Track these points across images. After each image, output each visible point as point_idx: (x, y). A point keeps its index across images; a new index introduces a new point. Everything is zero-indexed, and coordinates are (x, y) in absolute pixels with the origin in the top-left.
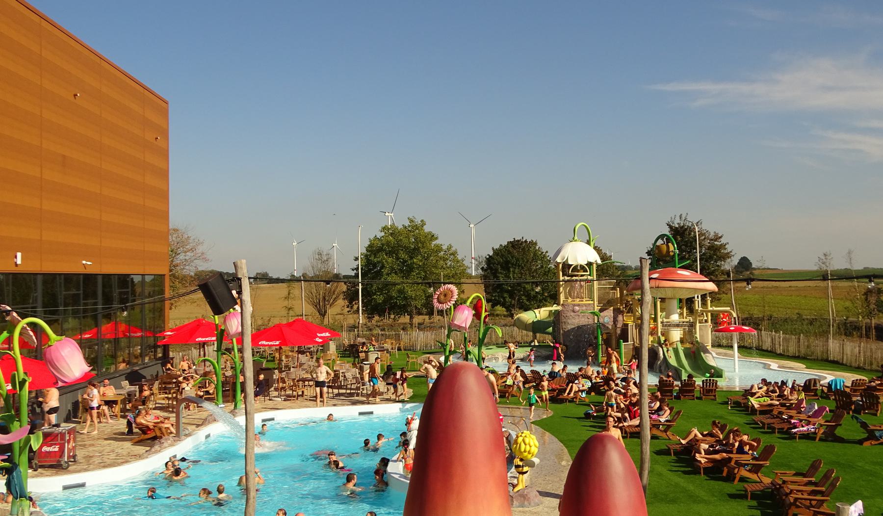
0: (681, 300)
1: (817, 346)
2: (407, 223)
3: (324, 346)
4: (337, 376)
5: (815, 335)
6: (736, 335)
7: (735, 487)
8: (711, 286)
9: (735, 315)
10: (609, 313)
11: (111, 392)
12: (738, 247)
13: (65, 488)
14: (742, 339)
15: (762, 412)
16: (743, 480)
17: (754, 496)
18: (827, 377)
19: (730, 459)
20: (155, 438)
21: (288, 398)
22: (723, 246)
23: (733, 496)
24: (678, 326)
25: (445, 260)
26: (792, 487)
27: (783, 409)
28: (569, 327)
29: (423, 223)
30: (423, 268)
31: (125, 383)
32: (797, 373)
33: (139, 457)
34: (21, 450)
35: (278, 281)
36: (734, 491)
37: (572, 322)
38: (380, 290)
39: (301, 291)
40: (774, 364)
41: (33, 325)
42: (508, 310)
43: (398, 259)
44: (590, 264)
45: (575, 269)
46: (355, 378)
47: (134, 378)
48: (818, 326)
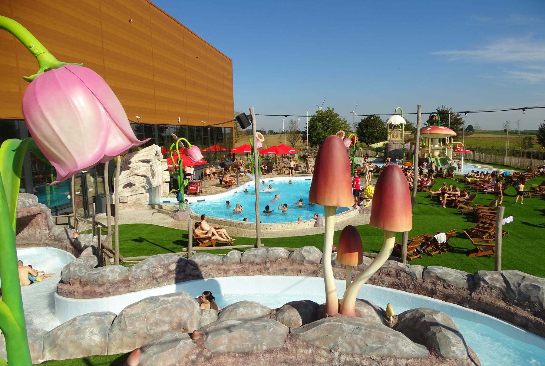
0: (440, 139)
1: (499, 160)
2: (327, 109)
3: (293, 155)
4: (297, 166)
5: (499, 155)
6: (463, 154)
7: (457, 210)
8: (453, 133)
9: (463, 145)
10: (409, 144)
11: (214, 170)
12: (467, 121)
13: (198, 201)
14: (466, 155)
15: (472, 184)
16: (461, 208)
17: (465, 214)
18: (502, 171)
19: (456, 199)
20: (230, 186)
21: (279, 174)
22: (461, 119)
23: (455, 214)
24: (438, 149)
25: (342, 124)
26: (482, 210)
27: (481, 182)
28: (392, 150)
29: (333, 109)
30: (333, 127)
31: (219, 167)
32: (490, 169)
33: (224, 192)
34: (181, 186)
35: (277, 133)
36: (456, 212)
37: (393, 148)
38: (316, 136)
39: (285, 136)
40: (479, 166)
41: (182, 141)
42: (367, 144)
43: (323, 124)
44: (401, 124)
45: (395, 126)
46: (304, 167)
47: (222, 165)
48: (501, 152)
